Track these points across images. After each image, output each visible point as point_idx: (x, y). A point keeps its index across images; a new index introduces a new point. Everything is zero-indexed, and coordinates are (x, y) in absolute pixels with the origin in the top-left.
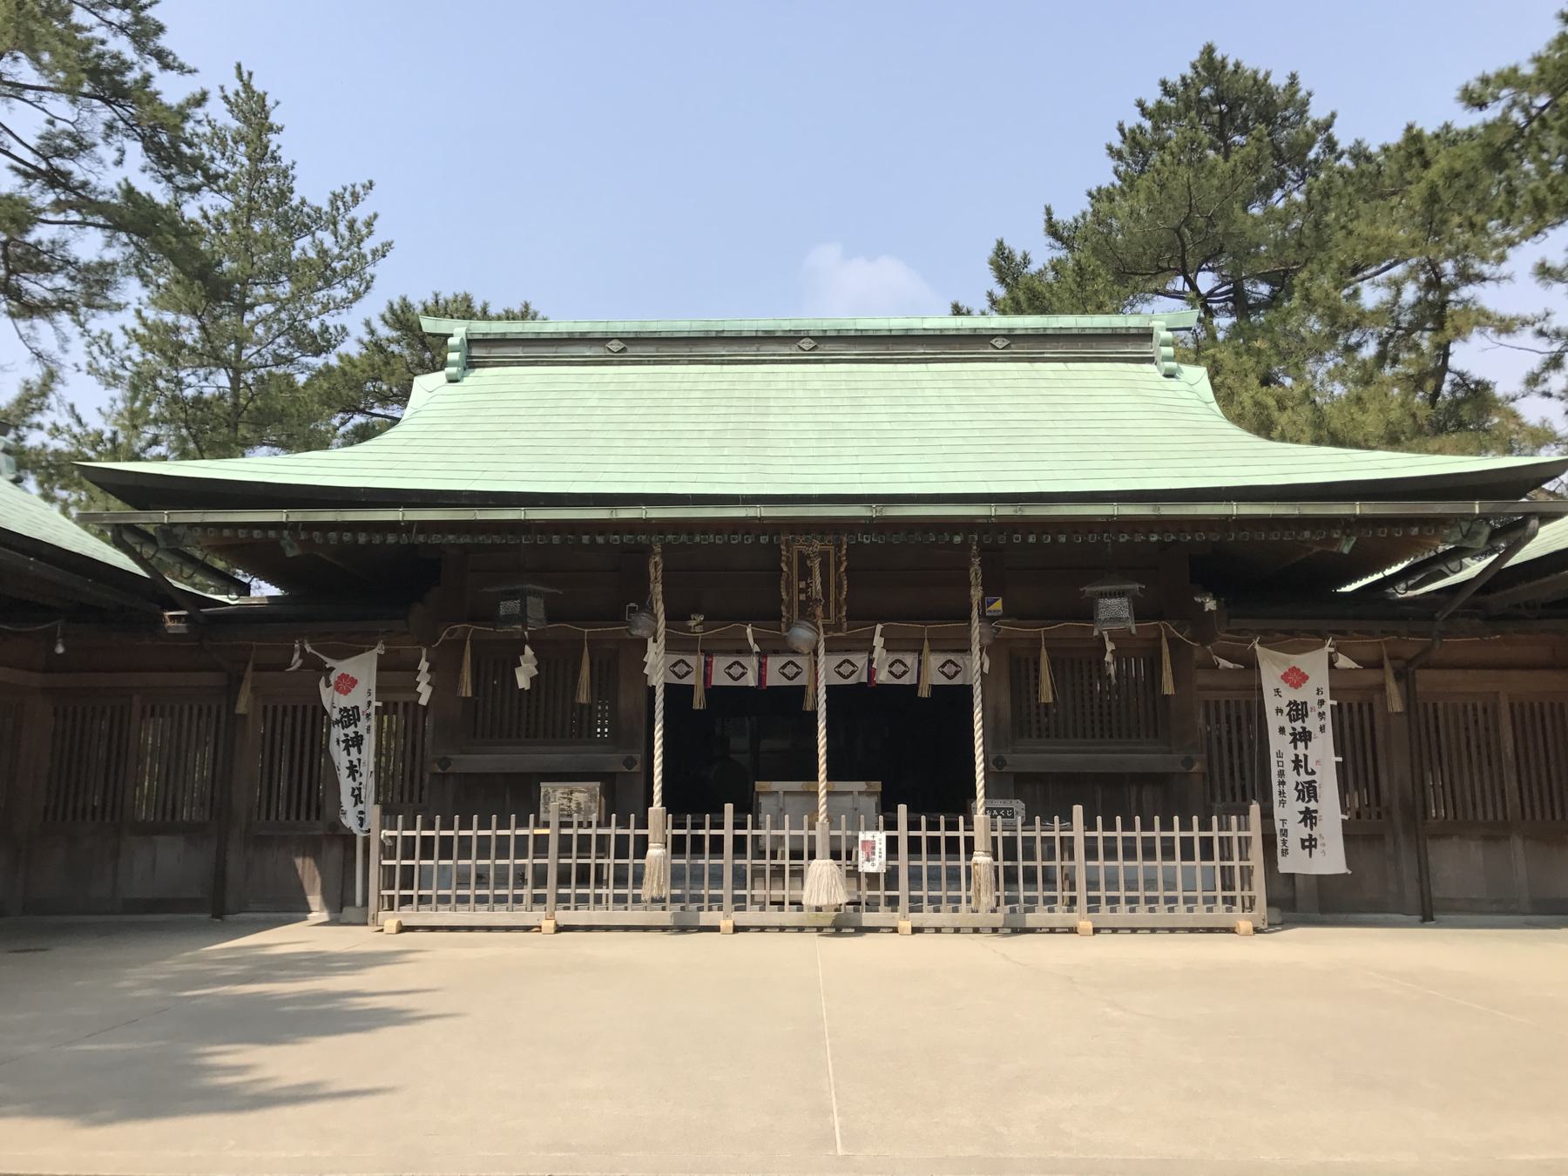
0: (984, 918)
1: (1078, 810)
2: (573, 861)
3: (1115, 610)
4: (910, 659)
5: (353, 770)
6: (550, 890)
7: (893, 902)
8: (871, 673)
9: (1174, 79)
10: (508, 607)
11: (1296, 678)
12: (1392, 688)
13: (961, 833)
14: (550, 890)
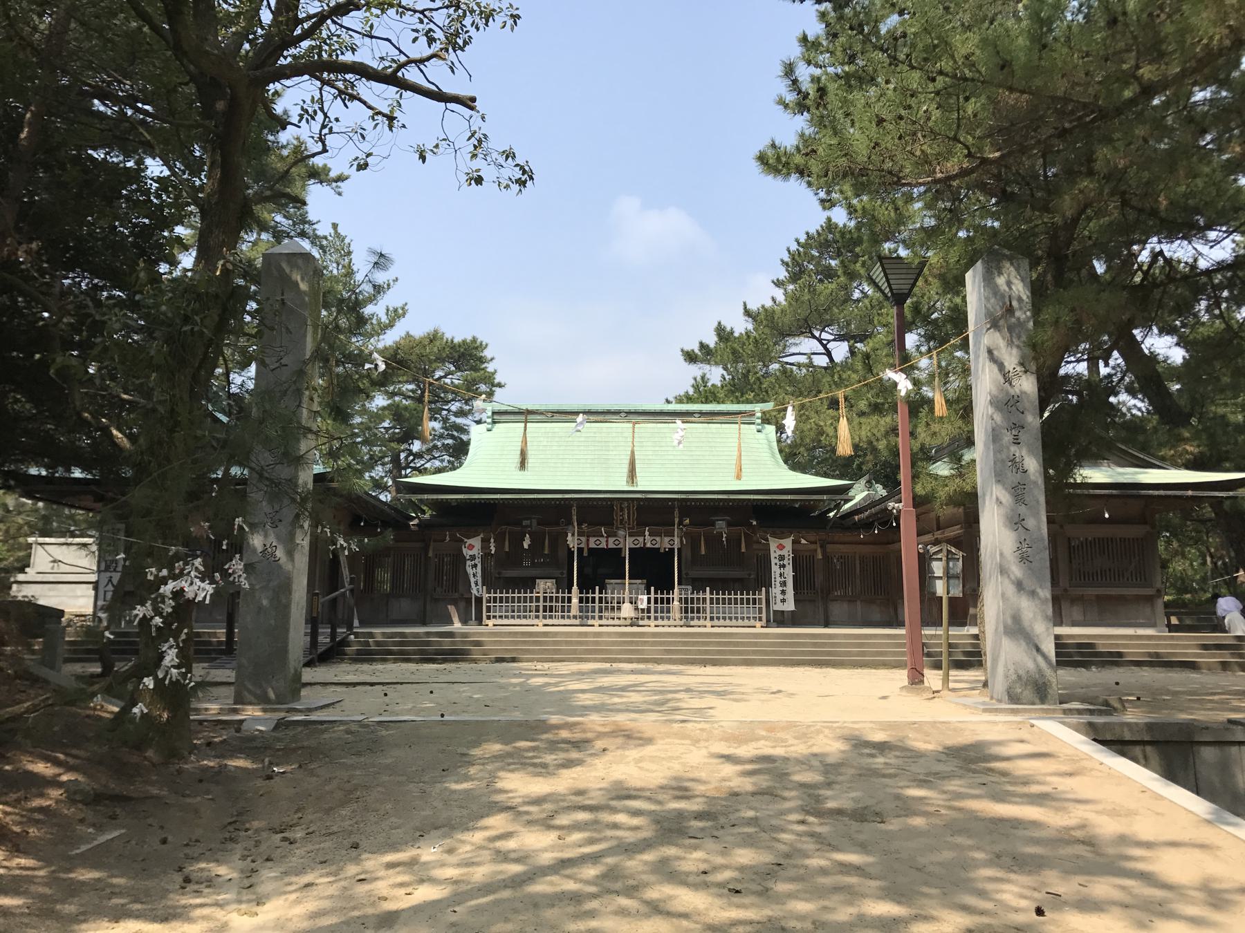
0: (678, 622)
1: (708, 589)
2: (548, 604)
3: (721, 525)
4: (658, 539)
5: (474, 575)
6: (541, 613)
7: (649, 618)
8: (645, 544)
9: (813, 231)
10: (525, 523)
11: (781, 547)
12: (819, 551)
13: (671, 596)
14: (541, 613)
